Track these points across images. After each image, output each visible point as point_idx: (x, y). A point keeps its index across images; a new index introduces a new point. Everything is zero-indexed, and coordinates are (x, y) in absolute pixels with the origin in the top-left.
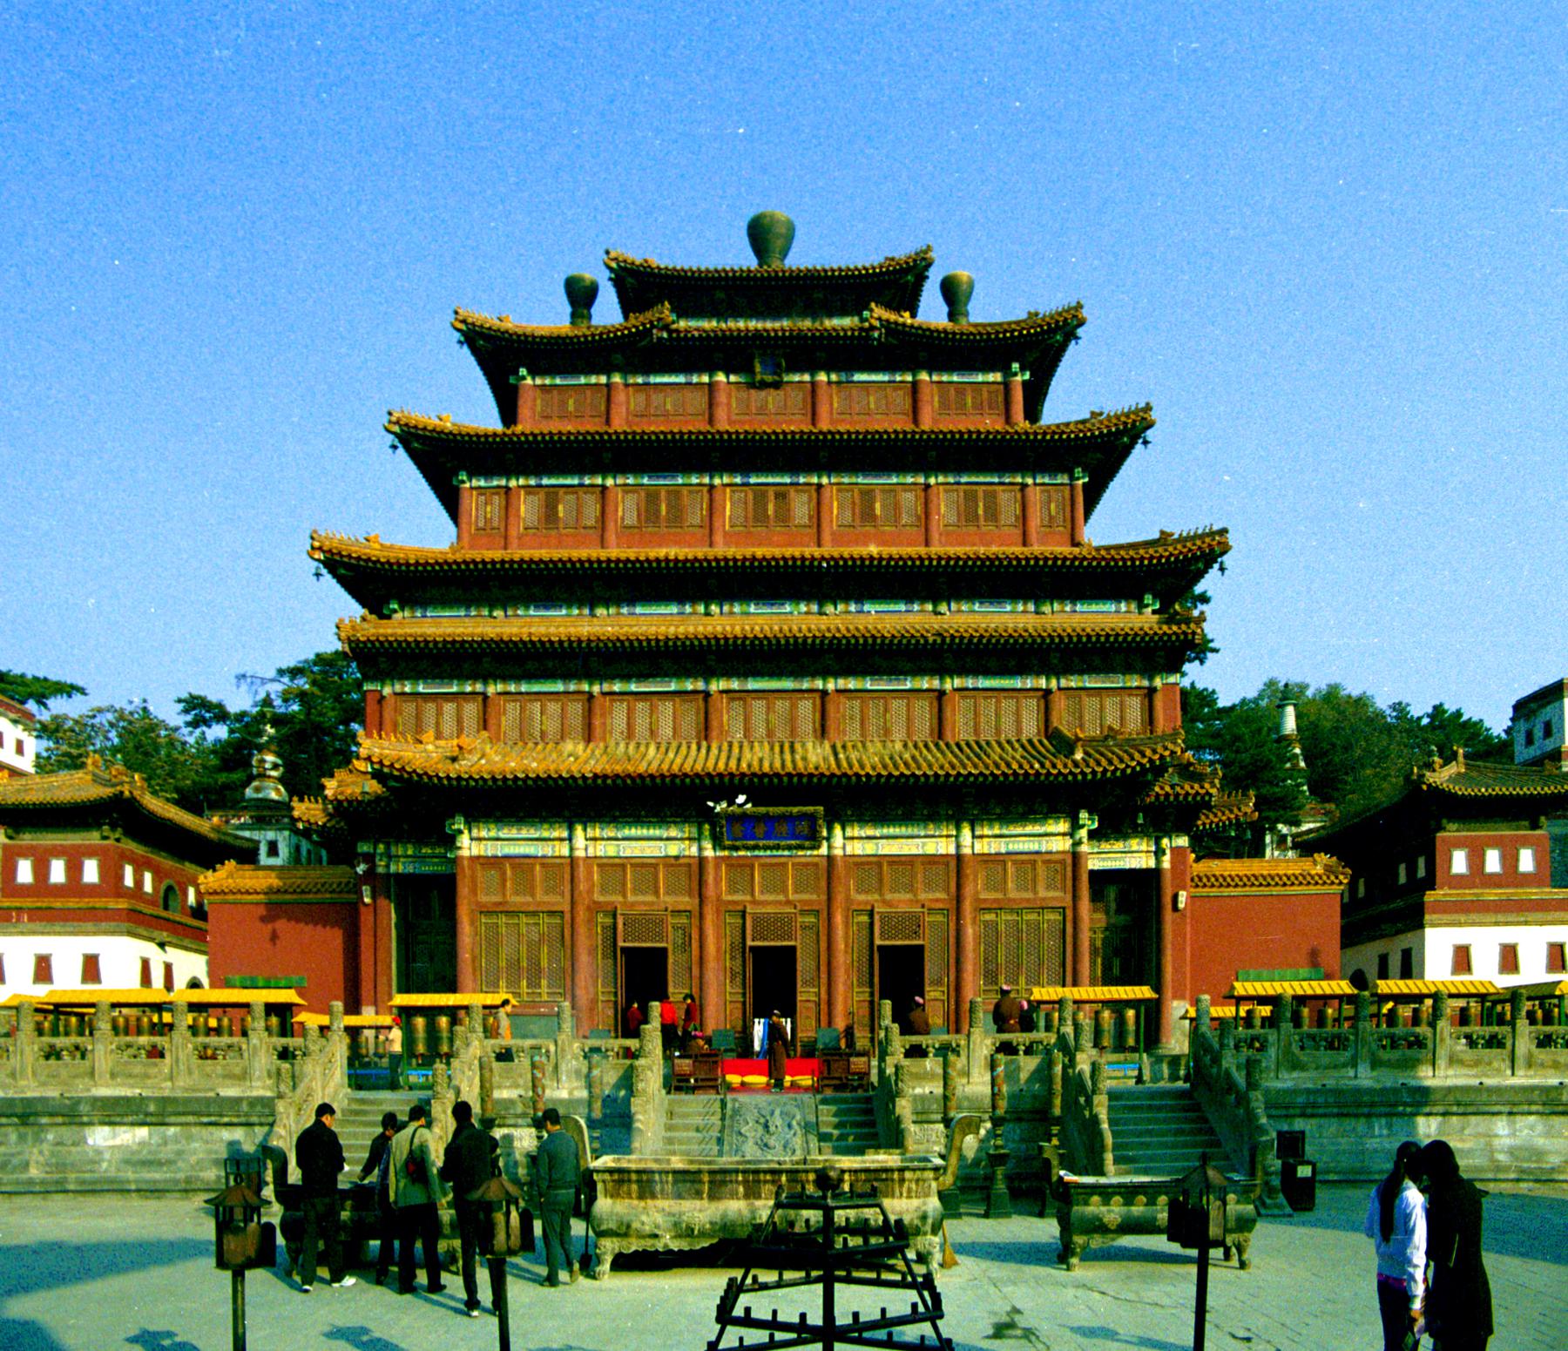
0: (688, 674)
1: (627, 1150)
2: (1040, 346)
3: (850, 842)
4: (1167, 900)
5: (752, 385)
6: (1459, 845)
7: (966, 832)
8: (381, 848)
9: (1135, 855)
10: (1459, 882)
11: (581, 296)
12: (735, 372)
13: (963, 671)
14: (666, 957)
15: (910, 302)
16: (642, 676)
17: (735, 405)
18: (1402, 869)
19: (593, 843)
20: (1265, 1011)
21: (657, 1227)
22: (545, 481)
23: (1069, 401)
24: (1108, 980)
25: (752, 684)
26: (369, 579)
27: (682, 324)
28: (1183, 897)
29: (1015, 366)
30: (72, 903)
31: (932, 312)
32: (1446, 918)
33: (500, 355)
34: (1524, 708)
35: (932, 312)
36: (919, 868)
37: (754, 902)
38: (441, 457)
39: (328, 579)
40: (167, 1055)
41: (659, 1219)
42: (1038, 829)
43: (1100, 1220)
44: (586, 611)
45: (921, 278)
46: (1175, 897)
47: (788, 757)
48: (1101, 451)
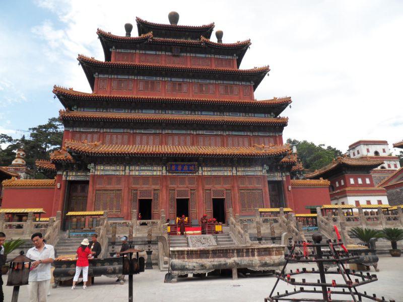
0: (157, 129)
1: (320, 243)
2: (240, 49)
3: (205, 172)
4: (286, 188)
5: (174, 56)
6: (351, 177)
7: (234, 169)
8: (65, 173)
9: (278, 177)
10: (352, 186)
11: (129, 28)
12: (168, 52)
13: (229, 130)
14: (141, 199)
15: (209, 36)
16: (145, 129)
17: (164, 60)
18: (337, 183)
19: (135, 171)
20: (376, 210)
21: (194, 267)
22: (119, 77)
23: (248, 63)
24: (272, 207)
25: (174, 132)
26: (67, 98)
27: (156, 38)
28: (290, 187)
29: (235, 55)
30: (356, 189)
31: (213, 39)
32: (352, 194)
33: (107, 41)
34: (352, 147)
35: (213, 39)
36: (151, 179)
37: (178, 187)
38: (89, 66)
39: (57, 99)
40: (366, 220)
41: (195, 264)
42: (253, 169)
43: (67, 273)
44: (129, 111)
45: (212, 30)
46: (288, 188)
47: (140, 147)
48: (257, 76)
